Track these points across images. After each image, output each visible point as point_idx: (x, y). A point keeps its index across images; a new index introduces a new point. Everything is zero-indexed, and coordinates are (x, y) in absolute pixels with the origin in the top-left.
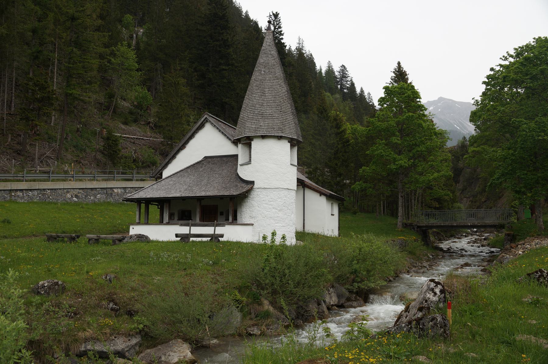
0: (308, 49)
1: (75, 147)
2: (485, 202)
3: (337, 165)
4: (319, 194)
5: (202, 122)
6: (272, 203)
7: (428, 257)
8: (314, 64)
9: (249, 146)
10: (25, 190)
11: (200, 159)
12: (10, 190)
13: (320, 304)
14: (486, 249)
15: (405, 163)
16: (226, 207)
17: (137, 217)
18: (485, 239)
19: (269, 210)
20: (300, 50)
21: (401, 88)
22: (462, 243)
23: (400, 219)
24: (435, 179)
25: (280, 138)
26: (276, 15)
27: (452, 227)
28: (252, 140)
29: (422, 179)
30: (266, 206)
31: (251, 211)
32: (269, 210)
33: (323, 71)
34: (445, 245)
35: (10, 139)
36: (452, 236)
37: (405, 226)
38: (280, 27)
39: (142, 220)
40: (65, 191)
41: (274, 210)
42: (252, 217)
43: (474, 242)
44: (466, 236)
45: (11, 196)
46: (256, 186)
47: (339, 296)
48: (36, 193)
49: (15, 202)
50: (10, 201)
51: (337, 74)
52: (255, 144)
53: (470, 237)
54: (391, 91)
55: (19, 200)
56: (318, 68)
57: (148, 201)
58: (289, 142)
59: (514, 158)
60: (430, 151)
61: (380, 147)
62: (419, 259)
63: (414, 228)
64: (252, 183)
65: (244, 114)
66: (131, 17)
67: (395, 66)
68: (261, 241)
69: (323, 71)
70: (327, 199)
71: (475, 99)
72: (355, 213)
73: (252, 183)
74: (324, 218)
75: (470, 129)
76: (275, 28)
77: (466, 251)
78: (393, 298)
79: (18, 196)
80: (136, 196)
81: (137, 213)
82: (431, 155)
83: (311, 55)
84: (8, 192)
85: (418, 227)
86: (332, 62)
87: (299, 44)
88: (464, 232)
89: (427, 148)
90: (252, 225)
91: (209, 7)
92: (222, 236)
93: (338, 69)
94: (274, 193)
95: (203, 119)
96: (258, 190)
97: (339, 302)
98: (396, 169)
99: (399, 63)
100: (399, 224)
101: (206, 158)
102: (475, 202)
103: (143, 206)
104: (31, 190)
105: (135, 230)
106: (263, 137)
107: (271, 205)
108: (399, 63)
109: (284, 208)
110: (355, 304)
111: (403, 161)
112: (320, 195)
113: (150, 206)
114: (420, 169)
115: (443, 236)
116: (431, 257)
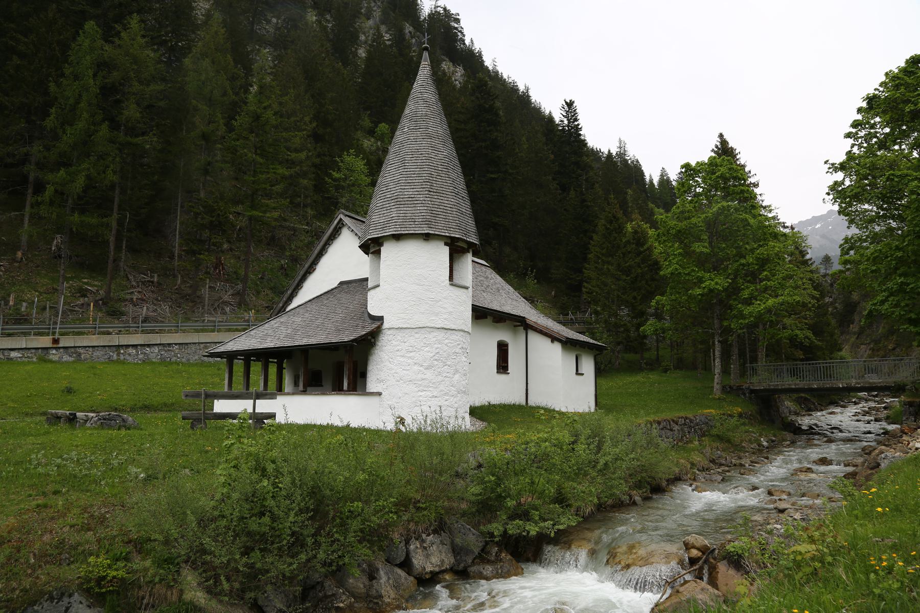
0: (633, 153)
1: (271, 289)
2: (894, 349)
3: (635, 298)
4: (550, 340)
5: (336, 227)
6: (412, 354)
7: (760, 445)
8: (642, 174)
9: (378, 253)
10: (141, 345)
11: (336, 285)
12: (119, 346)
13: (374, 578)
14: (875, 427)
15: (717, 283)
16: (342, 365)
17: (226, 382)
18: (885, 408)
19: (408, 368)
20: (622, 155)
21: (724, 172)
22: (844, 417)
23: (717, 378)
24: (769, 311)
25: (427, 237)
26: (570, 104)
27: (839, 389)
28: (381, 245)
29: (747, 310)
30: (402, 359)
31: (387, 366)
32: (408, 368)
33: (656, 182)
34: (805, 422)
35: (179, 282)
36: (835, 403)
37: (728, 390)
38: (576, 120)
39: (239, 387)
40: (202, 346)
41: (416, 368)
42: (380, 381)
43: (865, 413)
44: (855, 403)
45: (118, 354)
46: (386, 325)
47: (456, 550)
48: (156, 349)
49: (123, 362)
50: (118, 362)
51: (674, 183)
52: (387, 250)
53: (863, 404)
54: (694, 169)
55: (130, 359)
56: (647, 179)
57: (249, 356)
58: (446, 244)
59: (900, 254)
60: (764, 262)
61: (674, 261)
62: (737, 448)
63: (744, 394)
64: (381, 319)
65: (377, 202)
66: (387, 126)
67: (715, 141)
68: (390, 426)
69: (656, 182)
70: (563, 347)
71: (830, 162)
72: (665, 371)
73: (381, 319)
74: (560, 381)
75: (844, 230)
76: (569, 122)
77: (841, 431)
78: (593, 553)
79: (130, 355)
80: (222, 349)
81: (227, 376)
82: (764, 270)
83: (637, 161)
84: (114, 349)
85: (752, 391)
86: (666, 169)
87: (620, 148)
88: (854, 397)
89: (758, 259)
90: (380, 394)
91: (473, 98)
92: (272, 416)
93: (675, 178)
94: (417, 336)
95: (336, 222)
96: (389, 332)
97: (458, 562)
98: (702, 295)
99: (721, 136)
100: (717, 387)
101: (341, 283)
102: (878, 350)
103: (239, 365)
104: (149, 346)
105: (221, 406)
106: (397, 237)
107: (410, 357)
108: (721, 136)
109: (436, 363)
110: (488, 570)
111: (718, 282)
112: (552, 342)
113: (236, 361)
114: (746, 294)
115: (814, 404)
116: (765, 444)
